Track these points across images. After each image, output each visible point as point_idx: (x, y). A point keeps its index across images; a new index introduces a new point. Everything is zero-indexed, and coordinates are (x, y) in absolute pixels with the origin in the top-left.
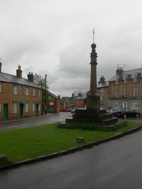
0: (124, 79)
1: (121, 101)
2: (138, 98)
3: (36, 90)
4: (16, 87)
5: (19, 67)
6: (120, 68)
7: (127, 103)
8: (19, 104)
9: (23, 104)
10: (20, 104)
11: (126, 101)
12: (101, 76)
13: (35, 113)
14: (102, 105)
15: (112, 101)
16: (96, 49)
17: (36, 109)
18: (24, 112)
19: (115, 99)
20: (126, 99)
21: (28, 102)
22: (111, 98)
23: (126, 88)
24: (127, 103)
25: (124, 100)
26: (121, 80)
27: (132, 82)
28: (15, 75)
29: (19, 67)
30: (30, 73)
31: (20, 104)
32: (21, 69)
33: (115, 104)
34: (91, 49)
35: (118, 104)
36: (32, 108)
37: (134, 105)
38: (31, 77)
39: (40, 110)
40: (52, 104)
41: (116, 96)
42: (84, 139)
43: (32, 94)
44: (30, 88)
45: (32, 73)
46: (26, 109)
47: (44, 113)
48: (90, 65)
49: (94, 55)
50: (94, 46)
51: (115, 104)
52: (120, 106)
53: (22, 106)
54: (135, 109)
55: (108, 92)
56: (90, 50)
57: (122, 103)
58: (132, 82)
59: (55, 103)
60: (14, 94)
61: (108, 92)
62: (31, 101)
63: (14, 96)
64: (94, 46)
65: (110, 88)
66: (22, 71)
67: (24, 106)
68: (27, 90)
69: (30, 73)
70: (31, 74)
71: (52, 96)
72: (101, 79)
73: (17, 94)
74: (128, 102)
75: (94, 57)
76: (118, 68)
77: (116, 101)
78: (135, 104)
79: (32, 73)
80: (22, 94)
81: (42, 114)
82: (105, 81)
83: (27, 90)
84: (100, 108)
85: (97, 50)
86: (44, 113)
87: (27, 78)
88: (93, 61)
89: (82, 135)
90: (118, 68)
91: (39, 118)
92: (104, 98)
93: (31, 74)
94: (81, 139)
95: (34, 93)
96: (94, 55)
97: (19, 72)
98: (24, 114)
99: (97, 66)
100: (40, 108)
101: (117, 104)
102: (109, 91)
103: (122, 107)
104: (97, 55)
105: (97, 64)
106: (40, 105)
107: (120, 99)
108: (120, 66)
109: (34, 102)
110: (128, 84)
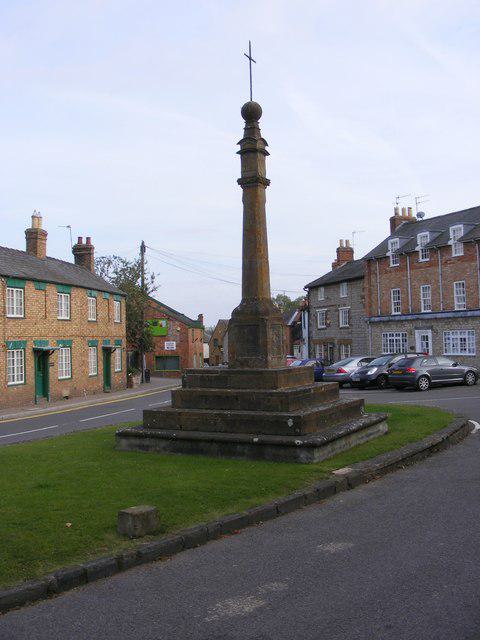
0: (418, 248)
1: (409, 326)
2: (469, 314)
4: (15, 290)
6: (403, 210)
7: (430, 336)
8: (100, 349)
9: (110, 348)
10: (36, 352)
11: (428, 328)
13: (101, 383)
14: (346, 346)
15: (377, 330)
17: (101, 367)
18: (112, 372)
20: (428, 319)
21: (67, 344)
22: (373, 319)
23: (427, 281)
24: (430, 336)
25: (420, 324)
26: (407, 253)
28: (23, 248)
30: (80, 239)
31: (36, 352)
33: (389, 338)
34: (242, 123)
35: (400, 338)
36: (85, 364)
37: (448, 341)
38: (83, 252)
40: (170, 345)
41: (393, 313)
42: (149, 513)
43: (84, 313)
44: (76, 292)
45: (88, 239)
46: (61, 368)
48: (239, 191)
49: (252, 149)
50: (251, 113)
51: (389, 338)
52: (407, 345)
53: (42, 357)
54: (460, 354)
55: (363, 297)
57: (411, 333)
58: (447, 257)
59: (183, 342)
60: (8, 316)
61: (363, 297)
63: (11, 323)
64: (251, 113)
65: (369, 283)
67: (52, 359)
68: (458, 305)
69: (80, 239)
70: (84, 242)
71: (172, 315)
72: (338, 250)
74: (435, 332)
75: (252, 155)
76: (396, 209)
77: (394, 330)
78: (459, 336)
79: (88, 239)
85: (265, 126)
86: (136, 380)
87: (71, 259)
88: (251, 174)
89: (184, 475)
92: (350, 318)
93: (84, 242)
94: (135, 516)
95: (92, 312)
96: (252, 149)
97: (35, 237)
98: (53, 388)
99: (268, 191)
100: (118, 363)
101: (395, 338)
102: (366, 293)
103: (413, 348)
104: (267, 148)
105: (267, 183)
106: (118, 352)
107: (405, 320)
108: (404, 204)
109: (93, 344)
110: (430, 264)
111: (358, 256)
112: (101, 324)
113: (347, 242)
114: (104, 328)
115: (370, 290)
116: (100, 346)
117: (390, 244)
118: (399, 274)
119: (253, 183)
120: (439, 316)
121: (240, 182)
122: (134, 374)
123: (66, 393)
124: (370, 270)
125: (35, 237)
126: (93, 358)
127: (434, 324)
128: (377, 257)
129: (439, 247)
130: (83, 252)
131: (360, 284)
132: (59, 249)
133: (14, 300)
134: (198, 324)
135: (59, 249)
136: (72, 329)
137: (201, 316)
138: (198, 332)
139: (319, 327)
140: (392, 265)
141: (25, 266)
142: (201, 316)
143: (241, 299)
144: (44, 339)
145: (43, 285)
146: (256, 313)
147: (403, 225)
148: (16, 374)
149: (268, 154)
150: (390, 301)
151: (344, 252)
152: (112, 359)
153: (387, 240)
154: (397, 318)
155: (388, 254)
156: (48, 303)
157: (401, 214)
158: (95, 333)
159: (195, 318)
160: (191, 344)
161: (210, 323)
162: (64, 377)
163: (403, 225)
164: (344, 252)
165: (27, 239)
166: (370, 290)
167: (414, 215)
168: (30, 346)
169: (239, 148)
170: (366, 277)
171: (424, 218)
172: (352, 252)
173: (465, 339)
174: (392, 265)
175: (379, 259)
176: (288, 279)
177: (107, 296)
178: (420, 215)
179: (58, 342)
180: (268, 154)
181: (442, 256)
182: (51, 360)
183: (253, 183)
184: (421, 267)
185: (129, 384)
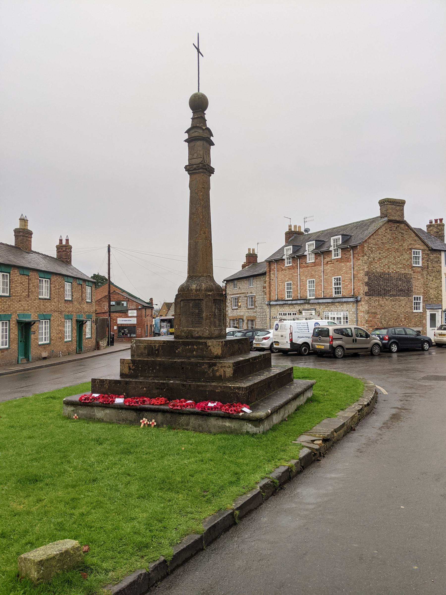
3: (75, 284)
4: (44, 280)
5: (24, 220)
6: (295, 226)
8: (74, 321)
10: (19, 323)
12: (249, 250)
13: (74, 346)
16: (208, 114)
17: (75, 335)
19: (283, 303)
22: (272, 303)
23: (312, 276)
25: (307, 306)
27: (328, 259)
29: (24, 220)
31: (19, 323)
32: (30, 227)
34: (190, 114)
36: (62, 332)
39: (88, 336)
43: (61, 293)
44: (54, 278)
45: (67, 240)
46: (42, 335)
47: (103, 343)
48: (186, 177)
49: (200, 137)
50: (199, 104)
53: (25, 328)
56: (186, 117)
62: (56, 313)
64: (199, 104)
66: (30, 233)
67: (33, 328)
70: (64, 243)
73: (8, 295)
79: (67, 240)
80: (25, 294)
81: (98, 347)
82: (258, 261)
83: (68, 286)
84: (226, 327)
86: (103, 343)
88: (199, 161)
90: (290, 226)
91: (442, 318)
93: (64, 243)
96: (200, 137)
97: (23, 235)
98: (33, 352)
102: (267, 285)
106: (88, 323)
107: (295, 304)
109: (68, 317)
110: (315, 264)
111: (260, 260)
112: (75, 303)
113: (253, 250)
114: (78, 306)
115: (270, 283)
116: (75, 319)
117: (285, 250)
118: (292, 271)
119: (200, 170)
120: (321, 301)
121: (187, 168)
122: (102, 339)
123: (44, 355)
124: (270, 269)
125: (23, 235)
126: (68, 329)
127: (317, 307)
128: (275, 261)
129: (321, 251)
130: (64, 252)
131: (262, 278)
132: (44, 244)
133: (445, 339)
134: (149, 306)
135: (44, 244)
136: (50, 306)
137: (151, 299)
138: (148, 311)
139: (233, 308)
140: (286, 265)
141: (13, 258)
142: (151, 299)
143: (186, 275)
144: (26, 313)
145: (26, 272)
146: (201, 298)
147: (294, 237)
148: (44, 331)
149: (213, 144)
150: (284, 290)
151: (251, 258)
152: (84, 328)
153: (283, 248)
154: (290, 302)
155: (284, 258)
156: (31, 285)
157: (251, 253)
158: (71, 309)
159: (148, 301)
160: (144, 318)
161: (158, 305)
162: (44, 342)
163: (294, 237)
164: (251, 258)
165: (16, 236)
166: (270, 283)
167: (302, 230)
168: (14, 318)
169: (186, 136)
170: (268, 274)
171: (309, 233)
172: (257, 257)
173: (340, 318)
174: (286, 265)
175: (277, 261)
176: (225, 265)
177: (81, 282)
178: (306, 230)
179: (39, 316)
180: (213, 144)
181: (324, 258)
182: (32, 330)
183: (200, 170)
184: (308, 267)
185: (98, 347)
